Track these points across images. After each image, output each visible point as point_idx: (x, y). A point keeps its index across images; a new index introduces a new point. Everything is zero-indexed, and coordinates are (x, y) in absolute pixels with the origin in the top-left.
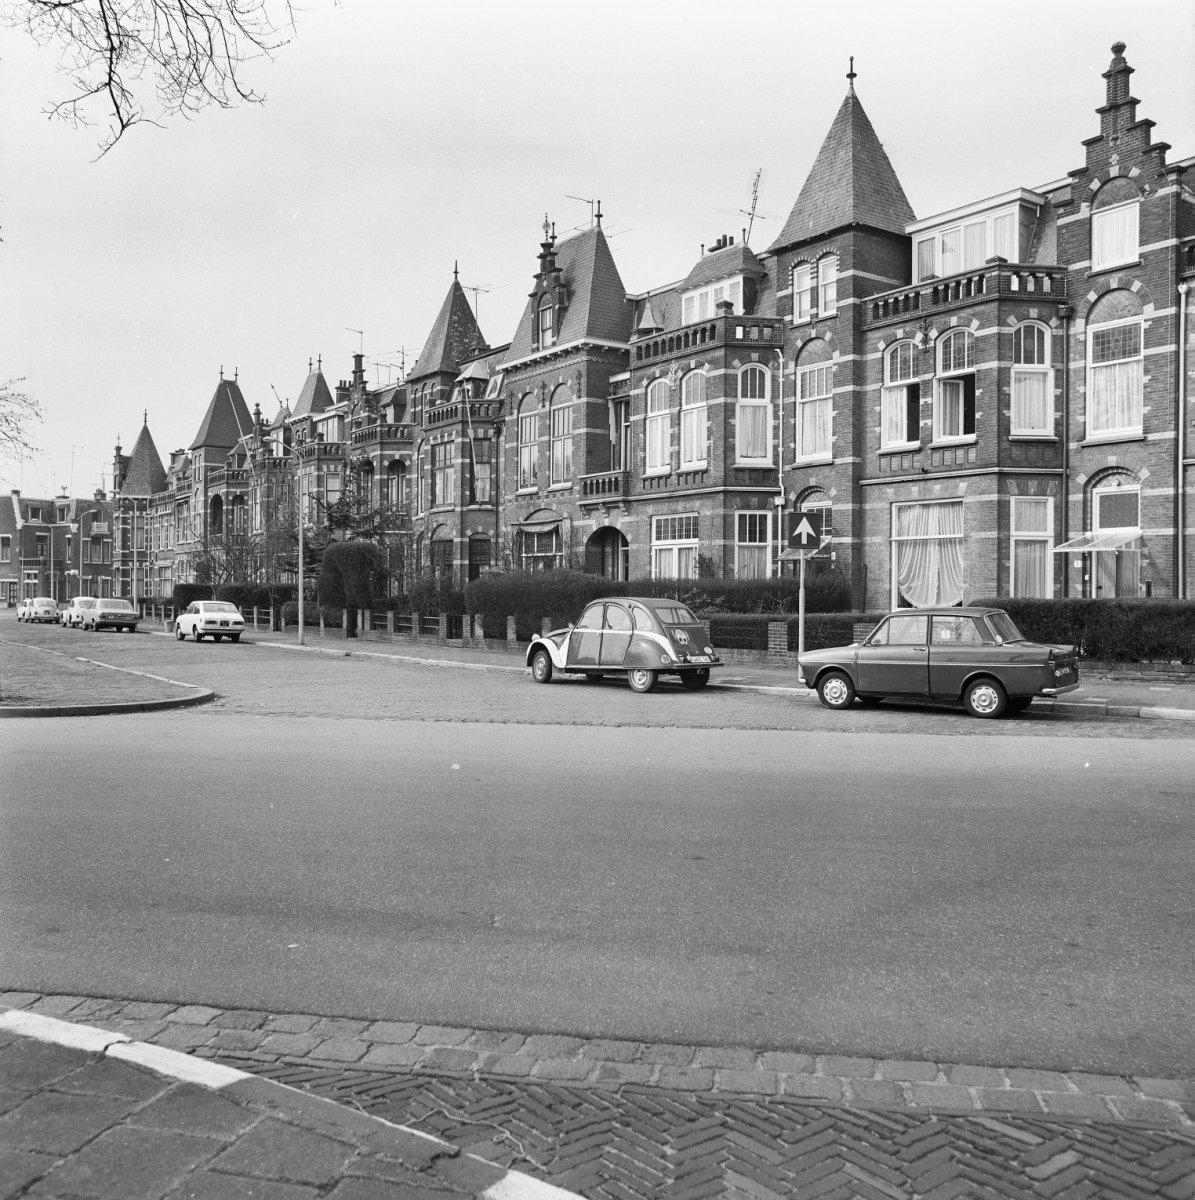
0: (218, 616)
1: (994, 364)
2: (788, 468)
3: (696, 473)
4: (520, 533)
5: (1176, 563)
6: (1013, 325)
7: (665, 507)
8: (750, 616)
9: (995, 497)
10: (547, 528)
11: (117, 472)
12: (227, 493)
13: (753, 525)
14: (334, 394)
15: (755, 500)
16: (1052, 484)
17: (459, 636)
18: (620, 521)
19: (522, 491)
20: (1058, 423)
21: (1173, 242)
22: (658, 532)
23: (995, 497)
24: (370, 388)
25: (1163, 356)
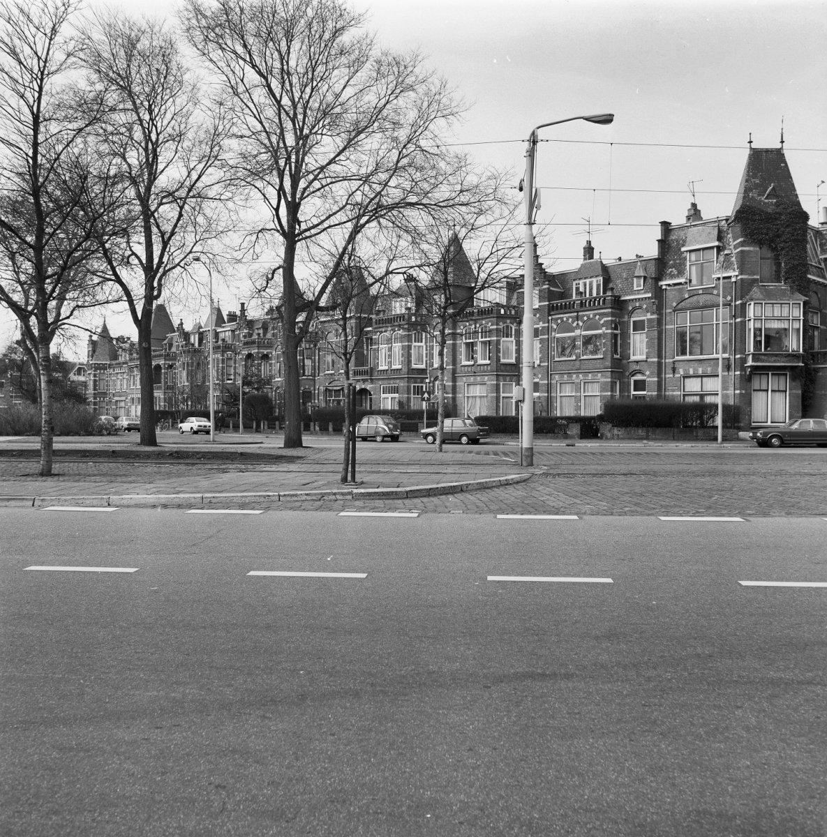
0: (203, 424)
1: (495, 338)
2: (431, 369)
3: (397, 370)
4: (326, 389)
5: (548, 405)
6: (501, 326)
7: (386, 382)
8: (413, 421)
9: (495, 382)
10: (338, 388)
11: (91, 349)
12: (165, 364)
13: (418, 389)
14: (226, 318)
15: (419, 380)
16: (515, 378)
17: (309, 430)
18: (369, 386)
19: (327, 372)
20: (516, 358)
21: (547, 303)
22: (383, 391)
23: (495, 382)
24: (248, 318)
25: (545, 339)
